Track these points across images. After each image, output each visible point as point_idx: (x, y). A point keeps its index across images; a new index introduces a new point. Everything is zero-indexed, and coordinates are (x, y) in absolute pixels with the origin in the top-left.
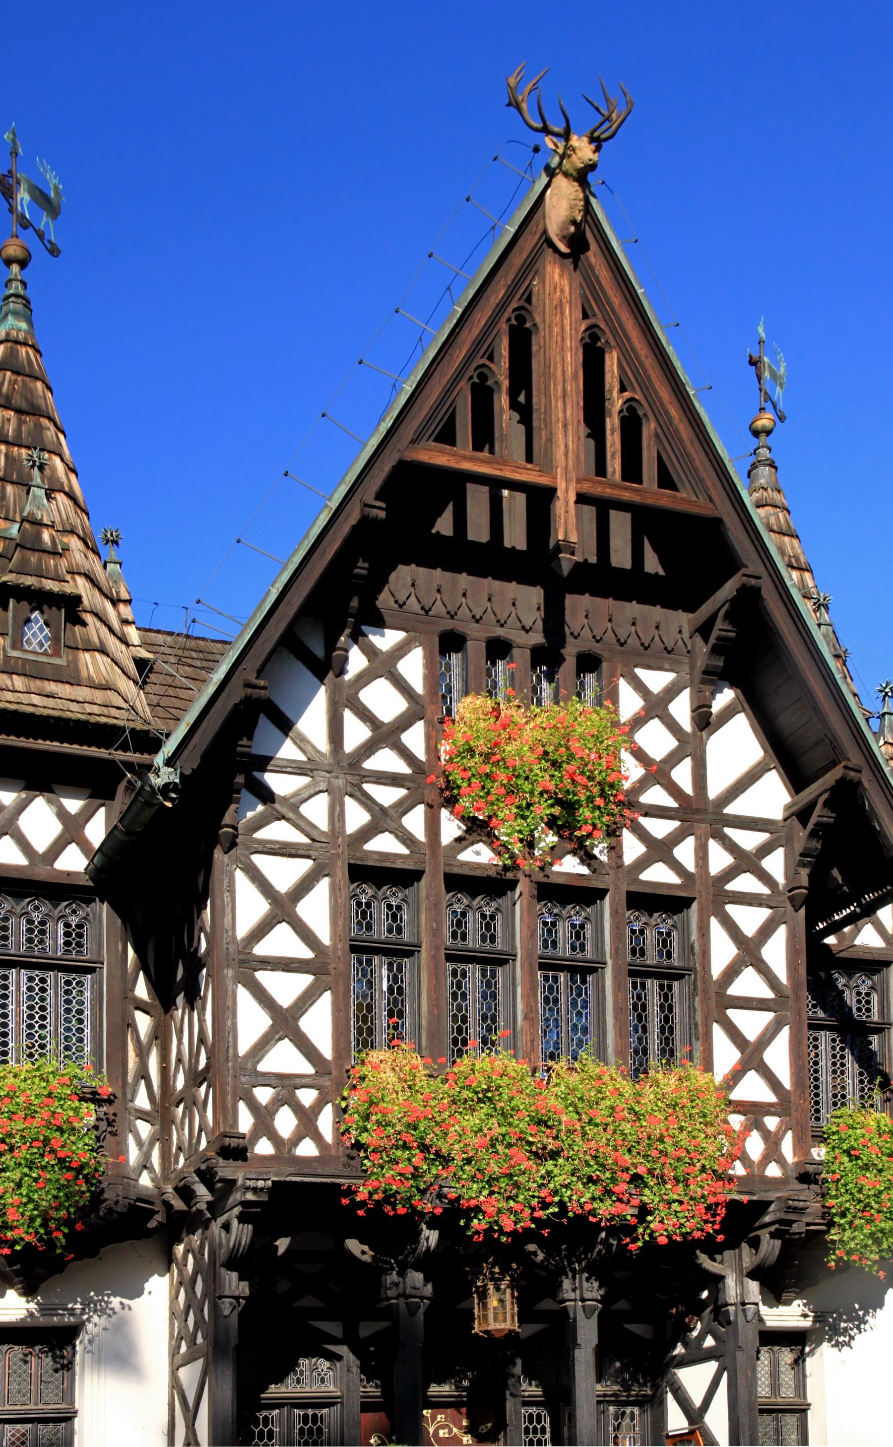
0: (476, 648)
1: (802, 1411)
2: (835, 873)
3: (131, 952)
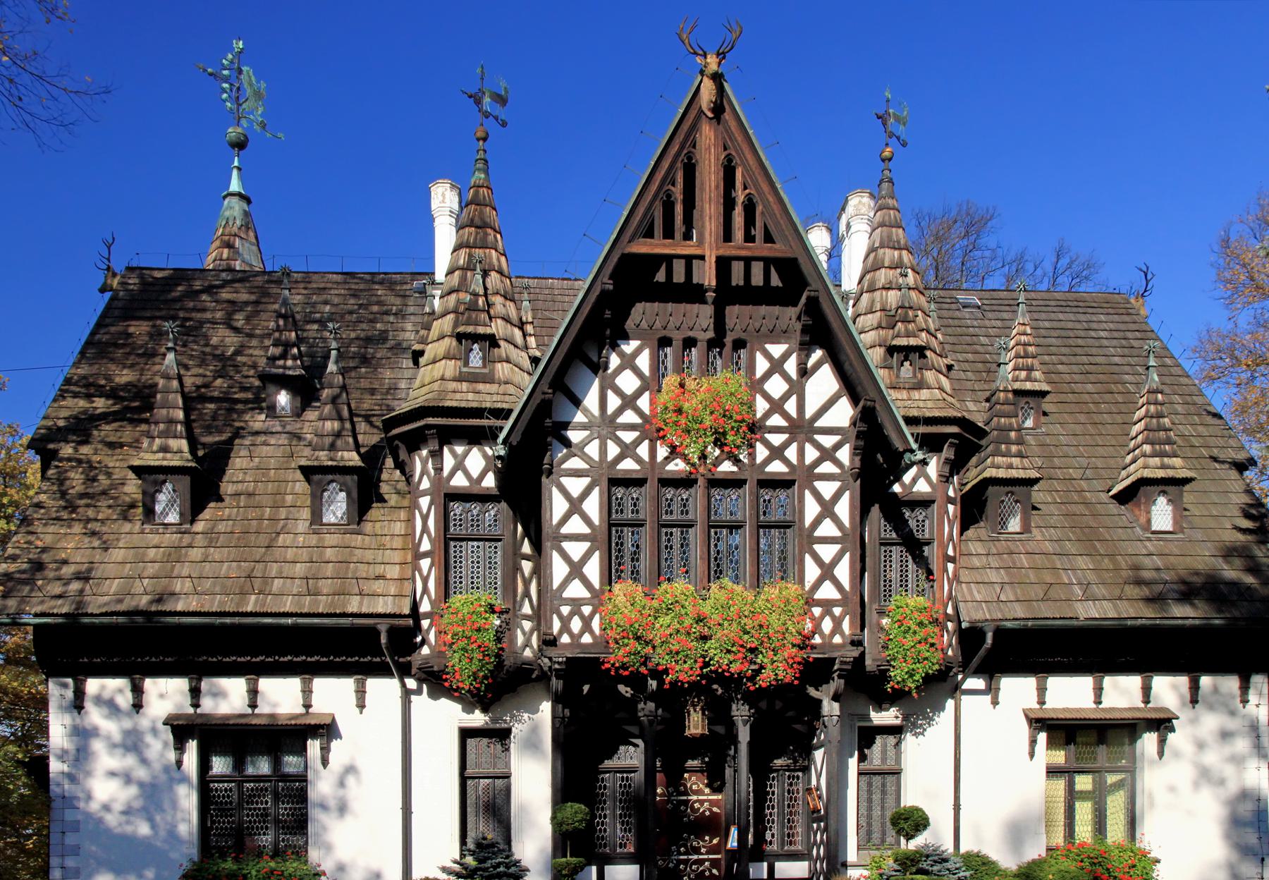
0: (677, 343)
1: (897, 773)
2: (879, 456)
3: (520, 528)
